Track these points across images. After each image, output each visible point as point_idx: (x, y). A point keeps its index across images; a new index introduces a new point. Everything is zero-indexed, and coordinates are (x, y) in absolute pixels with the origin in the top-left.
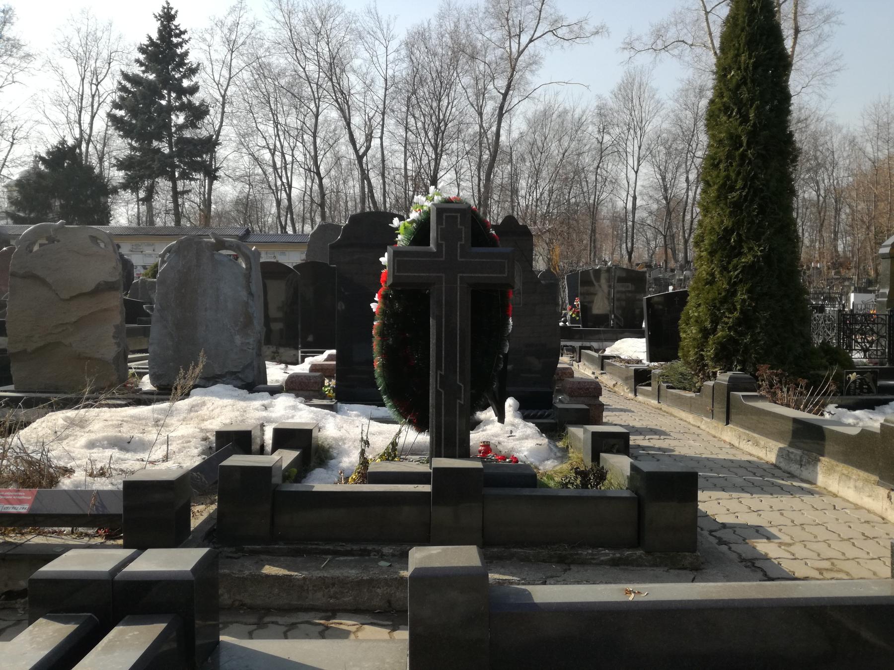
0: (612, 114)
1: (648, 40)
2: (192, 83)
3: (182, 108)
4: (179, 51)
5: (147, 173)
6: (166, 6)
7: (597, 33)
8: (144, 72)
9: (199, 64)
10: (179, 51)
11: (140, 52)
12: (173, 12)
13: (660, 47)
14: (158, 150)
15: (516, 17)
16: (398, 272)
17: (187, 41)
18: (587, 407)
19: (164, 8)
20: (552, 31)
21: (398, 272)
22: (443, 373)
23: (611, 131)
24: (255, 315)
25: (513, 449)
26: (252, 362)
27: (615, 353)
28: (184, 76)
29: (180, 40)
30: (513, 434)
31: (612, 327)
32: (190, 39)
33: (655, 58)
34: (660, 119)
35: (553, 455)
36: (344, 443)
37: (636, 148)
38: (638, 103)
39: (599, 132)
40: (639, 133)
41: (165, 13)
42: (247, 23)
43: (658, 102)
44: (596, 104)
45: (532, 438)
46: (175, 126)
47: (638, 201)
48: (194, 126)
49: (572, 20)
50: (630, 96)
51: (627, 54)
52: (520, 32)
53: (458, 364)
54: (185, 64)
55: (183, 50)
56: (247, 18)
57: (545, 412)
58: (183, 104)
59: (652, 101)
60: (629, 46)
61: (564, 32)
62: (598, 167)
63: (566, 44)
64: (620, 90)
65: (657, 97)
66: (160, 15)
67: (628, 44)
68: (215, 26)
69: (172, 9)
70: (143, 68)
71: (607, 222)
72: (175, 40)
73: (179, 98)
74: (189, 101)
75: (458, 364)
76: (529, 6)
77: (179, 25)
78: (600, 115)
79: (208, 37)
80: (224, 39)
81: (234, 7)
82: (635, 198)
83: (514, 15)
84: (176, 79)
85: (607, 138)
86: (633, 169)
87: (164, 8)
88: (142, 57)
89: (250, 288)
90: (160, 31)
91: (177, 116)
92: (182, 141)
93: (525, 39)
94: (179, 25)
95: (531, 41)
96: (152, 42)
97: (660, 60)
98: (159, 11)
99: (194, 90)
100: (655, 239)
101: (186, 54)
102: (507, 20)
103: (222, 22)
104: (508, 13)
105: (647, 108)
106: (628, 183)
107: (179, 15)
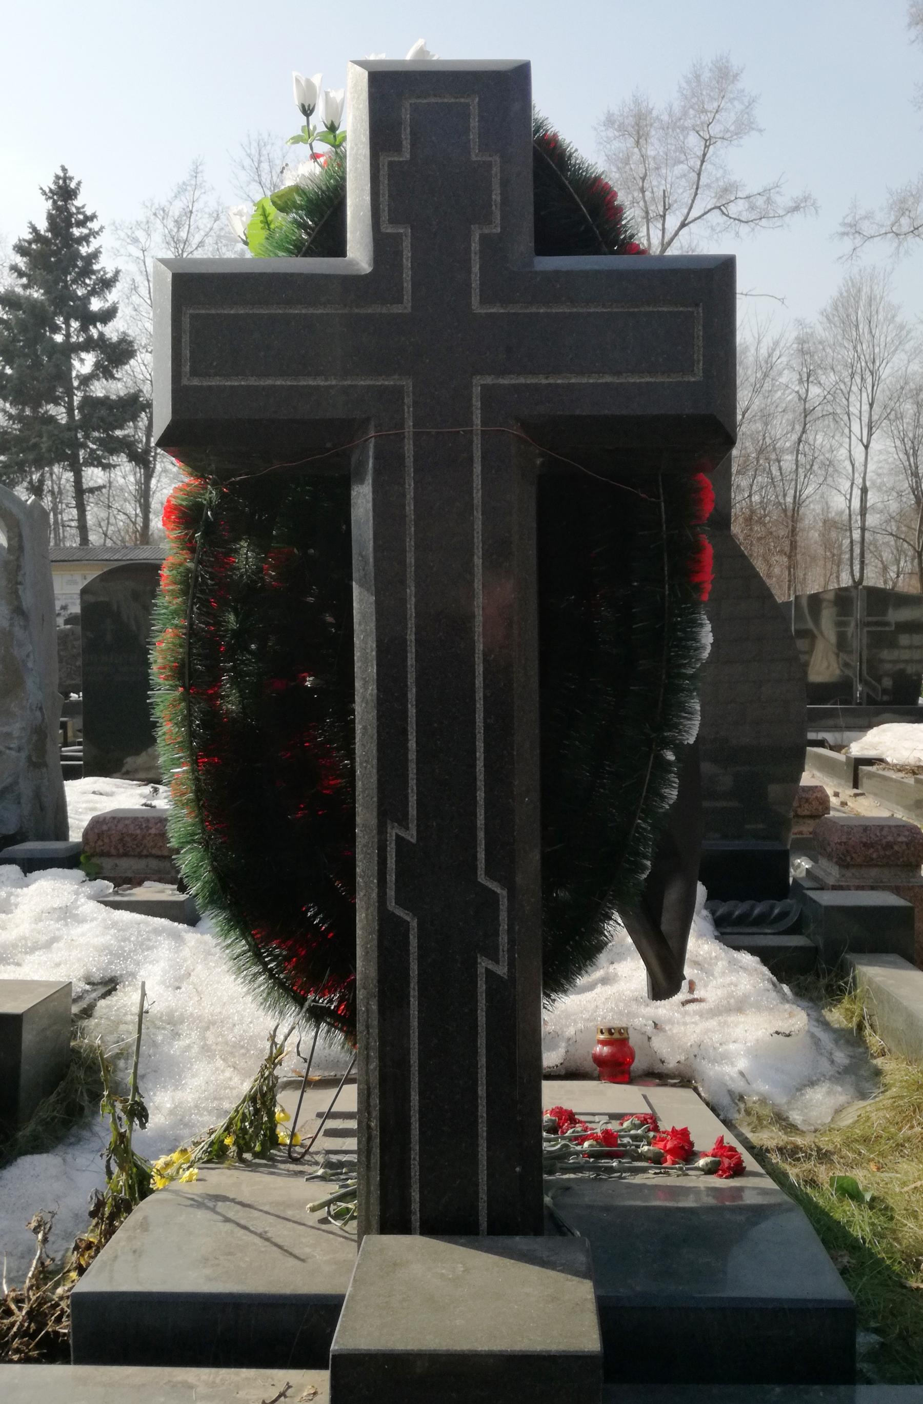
0: (824, 349)
1: (884, 218)
2: (107, 305)
3: (89, 345)
4: (84, 250)
5: (31, 457)
6: (62, 175)
7: (796, 208)
8: (25, 287)
9: (117, 272)
10: (84, 250)
11: (17, 252)
12: (73, 185)
13: (905, 229)
14: (52, 420)
15: (658, 187)
16: (194, 373)
17: (97, 233)
18: (908, 904)
19: (58, 177)
20: (719, 208)
21: (194, 373)
22: (411, 835)
23: (823, 379)
24: (30, 665)
25: (699, 1051)
26: (16, 783)
27: (871, 753)
28: (93, 292)
29: (85, 231)
30: (696, 995)
31: (860, 704)
32: (102, 228)
33: (898, 248)
34: (904, 356)
35: (825, 1065)
36: (176, 1035)
37: (866, 407)
38: (866, 330)
39: (801, 381)
40: (869, 380)
41: (60, 187)
42: (207, 210)
43: (902, 327)
44: (794, 334)
45: (758, 1008)
46: (77, 376)
47: (870, 495)
48: (109, 375)
49: (752, 187)
50: (853, 318)
51: (847, 244)
52: (665, 210)
53: (481, 795)
54: (93, 272)
55: (91, 249)
56: (206, 203)
57: (772, 908)
58: (89, 339)
59: (892, 326)
60: (852, 229)
61: (740, 209)
62: (800, 441)
63: (744, 229)
64: (837, 310)
65: (898, 319)
66: (51, 191)
67: (851, 226)
68: (152, 217)
69: (71, 179)
70: (24, 280)
71: (815, 535)
72: (77, 232)
73: (84, 328)
74: (101, 335)
75: (481, 795)
76: (681, 166)
77: (83, 207)
78: (802, 352)
79: (141, 234)
80: (169, 239)
81: (184, 183)
82: (864, 491)
83: (655, 183)
84: (79, 298)
85: (814, 390)
86: (861, 441)
87: (58, 177)
88: (21, 262)
89: (18, 597)
90: (50, 217)
91: (82, 361)
92: (90, 403)
93: (672, 222)
94: (83, 207)
95: (683, 225)
96: (38, 237)
97: (906, 252)
98: (49, 183)
99: (108, 315)
100: (898, 562)
101: (95, 255)
102: (643, 191)
103: (164, 211)
104: (643, 179)
105: (883, 339)
106: (853, 465)
107: (82, 189)
